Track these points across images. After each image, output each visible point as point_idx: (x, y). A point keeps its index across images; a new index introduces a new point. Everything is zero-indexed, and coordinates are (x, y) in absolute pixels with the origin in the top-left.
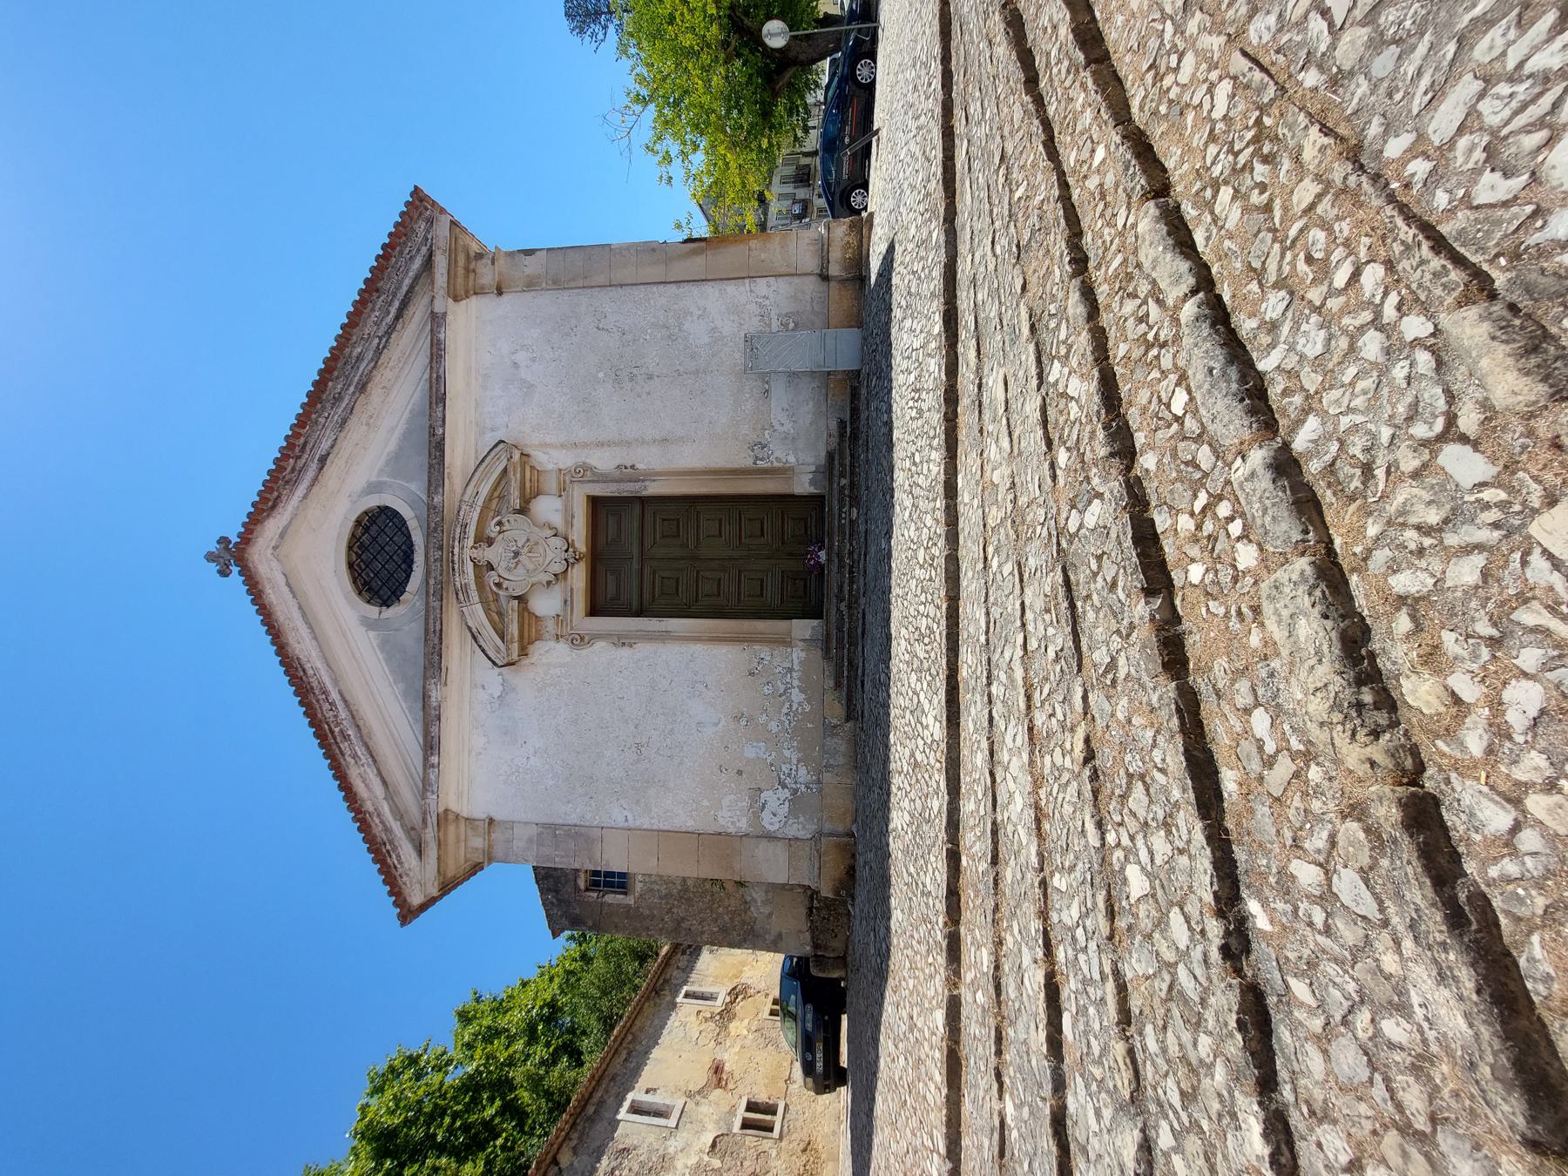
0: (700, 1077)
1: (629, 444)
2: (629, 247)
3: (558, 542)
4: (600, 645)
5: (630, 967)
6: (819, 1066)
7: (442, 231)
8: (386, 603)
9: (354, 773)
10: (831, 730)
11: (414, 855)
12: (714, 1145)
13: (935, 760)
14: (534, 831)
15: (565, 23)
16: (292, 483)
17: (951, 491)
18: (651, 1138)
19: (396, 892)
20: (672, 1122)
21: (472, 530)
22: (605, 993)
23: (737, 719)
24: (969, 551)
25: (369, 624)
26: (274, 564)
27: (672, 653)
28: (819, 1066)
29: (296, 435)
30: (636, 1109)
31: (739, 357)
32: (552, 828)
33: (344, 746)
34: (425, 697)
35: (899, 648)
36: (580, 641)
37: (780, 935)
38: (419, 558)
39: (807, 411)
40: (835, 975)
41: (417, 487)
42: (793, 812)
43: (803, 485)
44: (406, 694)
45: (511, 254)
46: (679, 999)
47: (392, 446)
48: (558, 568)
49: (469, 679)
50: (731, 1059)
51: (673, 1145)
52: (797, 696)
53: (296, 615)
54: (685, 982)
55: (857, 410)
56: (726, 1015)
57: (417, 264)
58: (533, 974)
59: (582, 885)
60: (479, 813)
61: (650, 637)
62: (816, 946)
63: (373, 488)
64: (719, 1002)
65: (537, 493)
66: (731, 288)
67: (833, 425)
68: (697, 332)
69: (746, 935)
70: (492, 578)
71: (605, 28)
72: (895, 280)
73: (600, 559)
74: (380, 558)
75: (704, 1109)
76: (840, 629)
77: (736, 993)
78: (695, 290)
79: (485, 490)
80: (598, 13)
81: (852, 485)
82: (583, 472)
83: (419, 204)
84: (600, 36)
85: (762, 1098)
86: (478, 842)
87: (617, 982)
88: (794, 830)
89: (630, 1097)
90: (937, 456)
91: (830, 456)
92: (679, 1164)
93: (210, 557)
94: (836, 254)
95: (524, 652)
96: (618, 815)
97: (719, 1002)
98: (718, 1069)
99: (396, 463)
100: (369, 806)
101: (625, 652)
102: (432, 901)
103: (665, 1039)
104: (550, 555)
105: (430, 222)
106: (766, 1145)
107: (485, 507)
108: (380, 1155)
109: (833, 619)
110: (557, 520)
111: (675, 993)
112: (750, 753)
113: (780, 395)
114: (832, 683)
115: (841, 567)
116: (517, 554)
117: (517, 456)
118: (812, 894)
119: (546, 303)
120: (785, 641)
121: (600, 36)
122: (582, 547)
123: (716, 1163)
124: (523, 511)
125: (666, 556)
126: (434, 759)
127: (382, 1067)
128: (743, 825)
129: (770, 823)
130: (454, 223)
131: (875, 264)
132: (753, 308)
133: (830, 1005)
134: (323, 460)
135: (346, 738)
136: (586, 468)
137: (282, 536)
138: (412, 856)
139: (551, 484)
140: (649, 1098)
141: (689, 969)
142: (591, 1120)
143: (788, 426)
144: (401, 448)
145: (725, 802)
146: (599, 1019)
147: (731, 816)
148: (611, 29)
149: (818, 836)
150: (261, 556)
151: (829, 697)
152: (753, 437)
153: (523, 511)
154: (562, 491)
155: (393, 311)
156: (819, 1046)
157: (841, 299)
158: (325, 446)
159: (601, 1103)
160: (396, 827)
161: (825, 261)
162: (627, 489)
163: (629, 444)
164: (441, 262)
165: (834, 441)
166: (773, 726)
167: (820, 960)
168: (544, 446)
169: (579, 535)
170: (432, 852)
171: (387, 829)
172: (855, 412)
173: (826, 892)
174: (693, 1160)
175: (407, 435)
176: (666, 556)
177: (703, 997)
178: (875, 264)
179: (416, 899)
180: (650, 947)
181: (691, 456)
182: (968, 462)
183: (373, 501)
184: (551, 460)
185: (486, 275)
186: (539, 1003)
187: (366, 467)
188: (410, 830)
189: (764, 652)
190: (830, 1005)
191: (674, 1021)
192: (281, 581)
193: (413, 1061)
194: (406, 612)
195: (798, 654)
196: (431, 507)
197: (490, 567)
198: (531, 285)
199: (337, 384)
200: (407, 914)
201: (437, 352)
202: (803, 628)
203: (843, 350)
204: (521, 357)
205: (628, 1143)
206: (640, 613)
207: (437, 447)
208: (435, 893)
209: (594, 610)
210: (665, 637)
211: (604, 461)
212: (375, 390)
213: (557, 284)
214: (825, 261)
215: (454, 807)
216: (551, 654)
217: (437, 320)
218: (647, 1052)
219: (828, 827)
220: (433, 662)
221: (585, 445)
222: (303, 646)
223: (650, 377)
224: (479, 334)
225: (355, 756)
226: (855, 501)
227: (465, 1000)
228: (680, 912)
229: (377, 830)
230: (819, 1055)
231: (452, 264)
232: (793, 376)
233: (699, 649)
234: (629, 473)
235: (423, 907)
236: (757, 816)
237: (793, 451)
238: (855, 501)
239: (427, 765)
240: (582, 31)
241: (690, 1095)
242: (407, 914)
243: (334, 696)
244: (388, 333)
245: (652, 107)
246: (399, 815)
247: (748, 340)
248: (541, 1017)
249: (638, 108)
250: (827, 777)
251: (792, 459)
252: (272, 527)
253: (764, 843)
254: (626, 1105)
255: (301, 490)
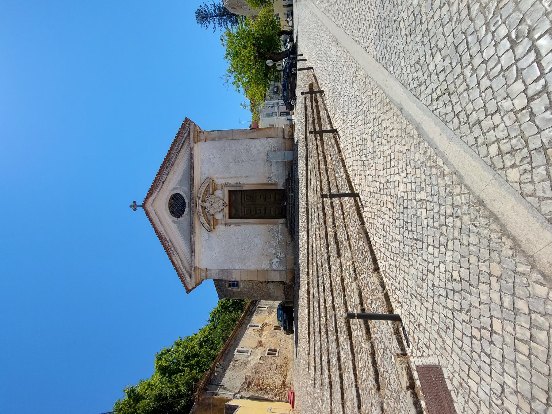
0: (255, 344)
1: (238, 177)
2: (238, 130)
3: (222, 201)
4: (232, 226)
5: (231, 323)
6: (288, 327)
7: (192, 127)
8: (178, 217)
9: (174, 258)
10: (288, 245)
11: (189, 277)
12: (260, 358)
13: (305, 243)
14: (217, 271)
15: (196, 21)
16: (156, 188)
17: (307, 196)
18: (244, 358)
19: (185, 286)
20: (249, 354)
21: (201, 199)
22: (223, 331)
23: (266, 243)
24: (310, 207)
25: (174, 222)
26: (152, 208)
27: (250, 228)
28: (288, 327)
29: (157, 177)
30: (238, 351)
31: (264, 157)
32: (222, 270)
33: (171, 252)
34: (191, 239)
35: (300, 224)
36: (227, 225)
37: (277, 297)
38: (187, 206)
39: (281, 169)
40: (291, 306)
41: (186, 188)
42: (280, 264)
43: (280, 187)
44: (184, 239)
45: (208, 132)
46: (248, 327)
47: (179, 178)
48: (222, 208)
49: (201, 235)
50: (263, 340)
51: (249, 359)
52: (280, 237)
53: (158, 220)
54: (249, 323)
55: (292, 168)
56: (262, 330)
57: (186, 135)
58: (197, 332)
59: (227, 286)
60: (204, 267)
61: (245, 224)
62: (286, 299)
63: (175, 189)
64: (259, 327)
65: (216, 189)
66: (262, 140)
67: (287, 172)
68: (254, 151)
69: (269, 297)
70: (206, 210)
71: (209, 22)
72: (299, 144)
73: (232, 205)
74: (177, 206)
75: (257, 351)
76: (290, 221)
77: (264, 325)
78: (253, 141)
79: (204, 189)
80: (207, 17)
81: (292, 188)
82: (227, 185)
83: (186, 119)
84: (208, 24)
85: (273, 348)
86: (204, 274)
87: (227, 328)
88: (280, 268)
89: (237, 349)
90: (305, 189)
91: (286, 180)
92: (252, 363)
93: (131, 206)
94: (287, 133)
95: (214, 228)
96: (238, 266)
97: (259, 327)
98: (260, 342)
99: (180, 182)
100: (178, 266)
101: (239, 227)
102: (194, 288)
103: (245, 336)
104: (220, 205)
105: (189, 125)
106: (274, 358)
107: (204, 193)
108: (164, 374)
109: (288, 218)
110: (221, 196)
111: (247, 325)
112: (269, 250)
113: (274, 165)
114: (290, 240)
115: (289, 206)
116: (212, 205)
117: (211, 181)
118: (284, 283)
119: (217, 143)
120: (277, 224)
121: (208, 24)
122: (227, 202)
123: (261, 362)
124: (213, 194)
125: (247, 204)
126: (193, 254)
127: (160, 353)
128: (268, 268)
129: (274, 267)
130: (195, 125)
131: (295, 142)
132: (267, 145)
133: (288, 318)
134: (163, 182)
135: (171, 250)
136: (228, 183)
137: (153, 201)
138: (189, 278)
139: (220, 188)
140: (242, 349)
141: (250, 319)
142: (227, 354)
143: (276, 173)
144: (181, 179)
145: (264, 262)
146: (222, 339)
147: (265, 266)
148: (211, 22)
149: (285, 270)
150: (148, 206)
151: (288, 237)
152: (268, 176)
153: (213, 194)
154: (222, 189)
155: (180, 146)
156: (287, 323)
157: (288, 143)
158: (164, 179)
159: (229, 350)
160: (184, 271)
161: (284, 135)
162: (238, 188)
163: (238, 177)
164: (192, 134)
165: (287, 177)
166: (275, 244)
167: (287, 302)
168: (217, 178)
169: (227, 200)
170: (193, 276)
171: (182, 271)
172: (292, 171)
173: (288, 283)
174: (255, 362)
175: (183, 176)
176: (247, 204)
177: (254, 326)
178: (295, 142)
179: (190, 288)
180: (236, 318)
181: (253, 180)
182: (309, 191)
183: (175, 192)
184: (219, 181)
185: (202, 137)
186: (203, 337)
187: (173, 183)
188: (187, 272)
189: (272, 227)
190: (288, 318)
191: (247, 332)
192: (154, 212)
193: (168, 351)
194: (184, 219)
195: (280, 227)
196: (191, 194)
197: (205, 208)
198: (213, 139)
199: (167, 164)
200: (188, 291)
201: (191, 156)
202: (281, 221)
203: (289, 156)
204: (211, 157)
205: (237, 359)
206: (241, 218)
207: (192, 179)
208: (194, 286)
209: (230, 218)
210: (248, 224)
211: (232, 182)
212: (175, 165)
213: (220, 139)
214: (284, 135)
215: (198, 266)
216: (220, 228)
217: (191, 149)
218: (240, 339)
219: (288, 267)
220: (192, 230)
221: (228, 178)
222: (160, 228)
223: (243, 161)
224: (202, 152)
225: (174, 254)
226: (292, 192)
227: (178, 340)
228: (252, 292)
229: (180, 271)
230: (287, 325)
231: (194, 134)
232: (277, 162)
233: (256, 226)
234: (238, 184)
235: (191, 290)
236: (271, 266)
237: (277, 179)
238: (292, 192)
239: (192, 256)
240: (201, 23)
241: (253, 348)
242: (188, 291)
243: (168, 240)
244: (179, 152)
245: (234, 73)
246: (184, 268)
247: (267, 154)
248: (204, 340)
249: (230, 74)
250: (287, 256)
251: (277, 181)
252: (151, 199)
253: (273, 272)
254: (236, 351)
255: (158, 190)
